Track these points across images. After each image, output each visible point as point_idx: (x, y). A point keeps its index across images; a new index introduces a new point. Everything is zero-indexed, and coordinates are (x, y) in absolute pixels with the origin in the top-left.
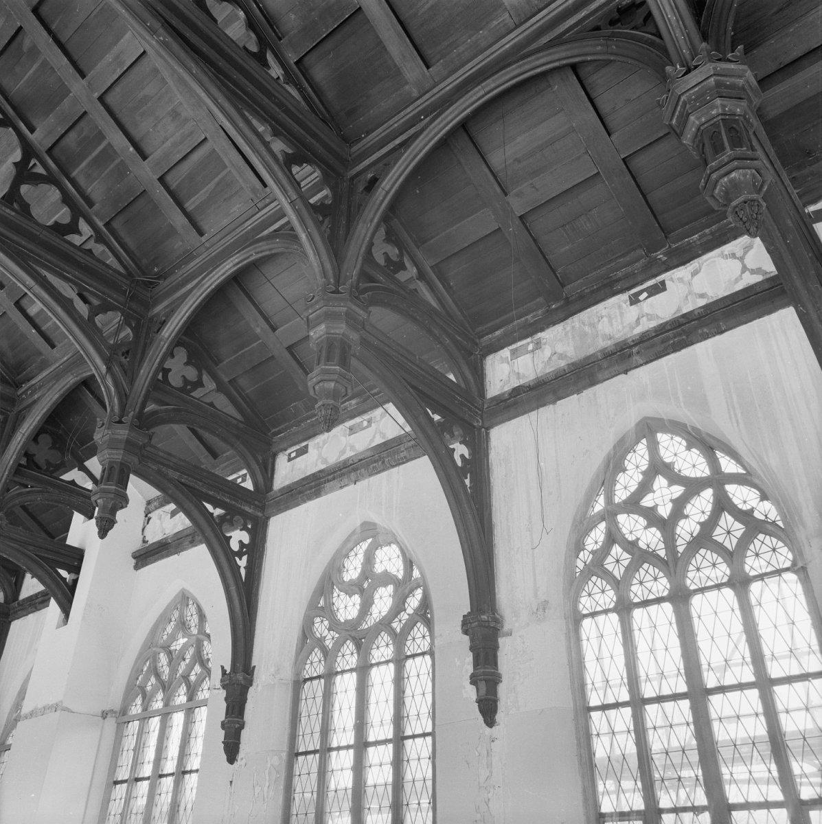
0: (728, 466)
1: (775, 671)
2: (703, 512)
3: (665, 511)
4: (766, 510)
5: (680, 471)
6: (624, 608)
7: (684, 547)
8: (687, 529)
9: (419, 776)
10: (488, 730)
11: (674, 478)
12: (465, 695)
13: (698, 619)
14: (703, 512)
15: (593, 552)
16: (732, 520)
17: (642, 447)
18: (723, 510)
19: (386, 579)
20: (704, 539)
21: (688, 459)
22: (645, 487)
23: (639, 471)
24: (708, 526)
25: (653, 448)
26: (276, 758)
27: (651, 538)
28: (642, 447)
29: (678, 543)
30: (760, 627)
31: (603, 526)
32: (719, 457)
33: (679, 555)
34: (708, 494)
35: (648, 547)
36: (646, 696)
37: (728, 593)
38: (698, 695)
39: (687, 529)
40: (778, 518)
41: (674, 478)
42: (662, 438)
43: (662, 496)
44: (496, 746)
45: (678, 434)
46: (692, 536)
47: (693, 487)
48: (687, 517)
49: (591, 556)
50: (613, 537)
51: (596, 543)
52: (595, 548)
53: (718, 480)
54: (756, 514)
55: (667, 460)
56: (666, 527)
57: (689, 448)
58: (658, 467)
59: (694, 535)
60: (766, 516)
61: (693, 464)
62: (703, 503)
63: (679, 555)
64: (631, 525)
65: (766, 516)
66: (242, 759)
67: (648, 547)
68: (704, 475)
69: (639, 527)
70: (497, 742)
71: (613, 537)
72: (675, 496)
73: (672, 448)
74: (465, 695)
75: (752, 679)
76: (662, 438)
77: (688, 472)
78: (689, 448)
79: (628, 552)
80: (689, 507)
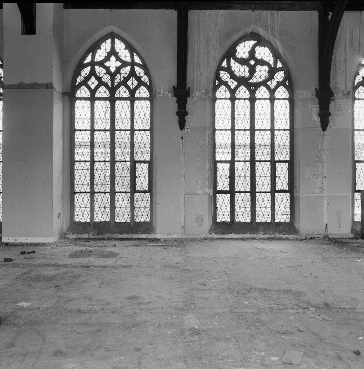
0: (137, 60)
1: (96, 128)
2: (126, 73)
3: (113, 69)
4: (145, 79)
5: (120, 56)
6: (93, 99)
7: (117, 83)
8: (119, 78)
9: (282, 143)
10: (322, 132)
11: (118, 59)
12: (313, 119)
13: (77, 108)
14: (126, 73)
15: (84, 77)
16: (135, 80)
17: (109, 41)
18: (132, 75)
19: (252, 71)
20: (124, 83)
21: (124, 53)
22: (107, 59)
23: (106, 51)
24: (127, 79)
25: (113, 43)
26: (209, 130)
27: (107, 79)
28: (109, 41)
29: (115, 82)
30: (216, 114)
31: (89, 68)
32: (134, 55)
33: (115, 86)
34: (129, 68)
35: (105, 81)
36: (76, 129)
37: (89, 102)
38: (253, 130)
39: (119, 78)
40: (148, 82)
41: (118, 59)
42: (117, 41)
43: (113, 64)
44: (325, 138)
45: (123, 42)
46: (120, 80)
47: (124, 64)
48: (120, 74)
49: (83, 78)
50: (93, 73)
51: (86, 74)
52: (85, 76)
53: (133, 64)
54: (142, 79)
55: (117, 51)
56: (112, 76)
57: (125, 49)
58: (113, 52)
59: (82, 81)
60: (145, 80)
61: (125, 55)
62: (127, 70)
63: (115, 86)
64: (99, 70)
65: (145, 80)
66: (188, 129)
67: (105, 81)
68: (128, 61)
69: (102, 73)
70: (326, 136)
71: (93, 73)
72: (118, 66)
73: (120, 46)
74: (313, 119)
75: (90, 129)
76: (117, 41)
77: (123, 58)
78: (125, 49)
79: (98, 81)
80: (121, 70)
